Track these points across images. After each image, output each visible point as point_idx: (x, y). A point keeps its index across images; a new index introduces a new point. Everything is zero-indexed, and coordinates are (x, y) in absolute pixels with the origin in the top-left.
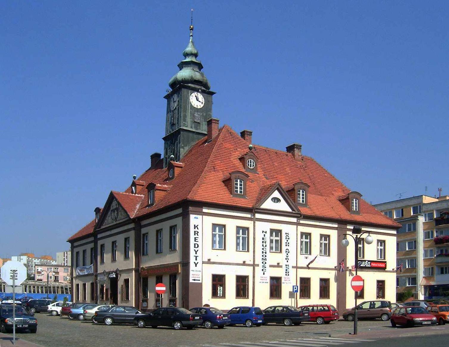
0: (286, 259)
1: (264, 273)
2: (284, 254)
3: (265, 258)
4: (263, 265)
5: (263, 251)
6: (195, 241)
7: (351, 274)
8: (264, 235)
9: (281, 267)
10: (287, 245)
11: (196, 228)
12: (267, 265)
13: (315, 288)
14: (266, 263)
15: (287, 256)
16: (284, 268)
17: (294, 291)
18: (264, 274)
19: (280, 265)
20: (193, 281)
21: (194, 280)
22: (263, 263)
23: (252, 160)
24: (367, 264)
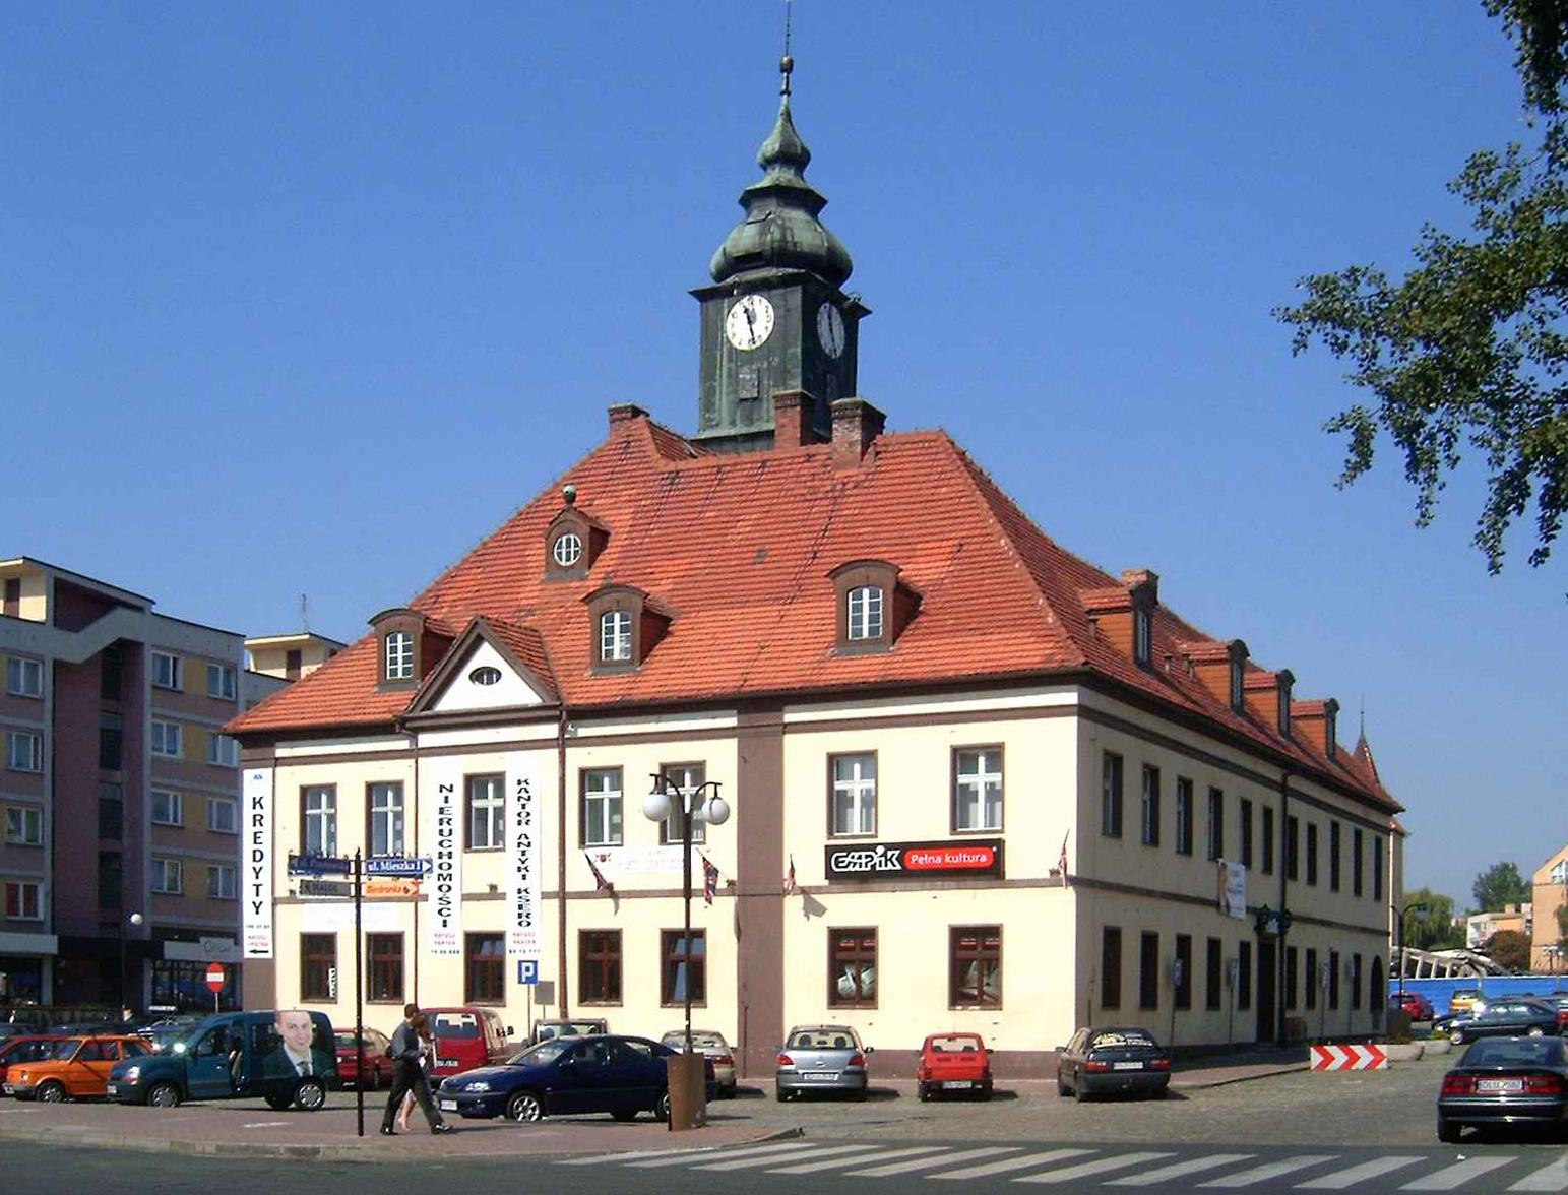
0: (519, 869)
1: (445, 921)
2: (512, 852)
3: (449, 872)
4: (441, 895)
5: (441, 849)
6: (255, 843)
7: (813, 909)
8: (447, 797)
9: (502, 897)
10: (524, 822)
11: (258, 805)
12: (455, 896)
13: (641, 966)
14: (450, 888)
15: (524, 858)
16: (513, 900)
17: (524, 980)
18: (445, 926)
19: (500, 891)
20: (253, 956)
21: (254, 952)
22: (440, 888)
23: (572, 536)
24: (883, 859)
